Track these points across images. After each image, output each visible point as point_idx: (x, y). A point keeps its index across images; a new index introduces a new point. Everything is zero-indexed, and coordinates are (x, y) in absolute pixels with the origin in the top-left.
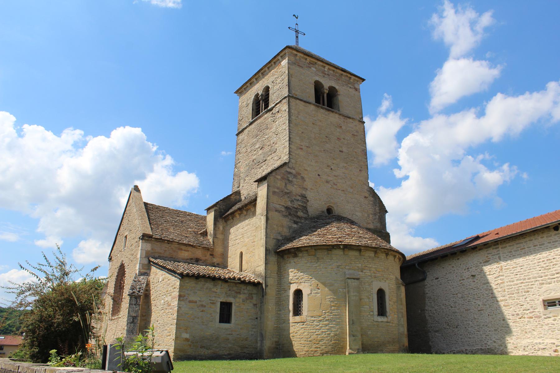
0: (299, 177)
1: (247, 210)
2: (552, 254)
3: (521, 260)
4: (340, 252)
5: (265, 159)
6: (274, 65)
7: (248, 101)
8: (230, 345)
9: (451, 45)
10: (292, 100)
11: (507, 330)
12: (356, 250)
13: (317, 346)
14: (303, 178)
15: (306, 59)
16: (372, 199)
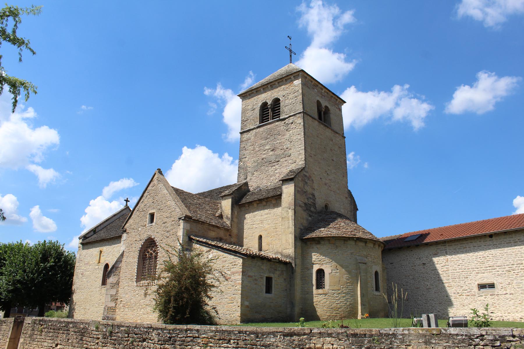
1: (267, 202)
2: (487, 253)
3: (463, 255)
4: (353, 243)
6: (285, 82)
7: (254, 105)
8: (272, 311)
9: (314, 33)
10: (305, 115)
11: (450, 303)
14: (313, 180)
15: (312, 82)
16: (349, 199)
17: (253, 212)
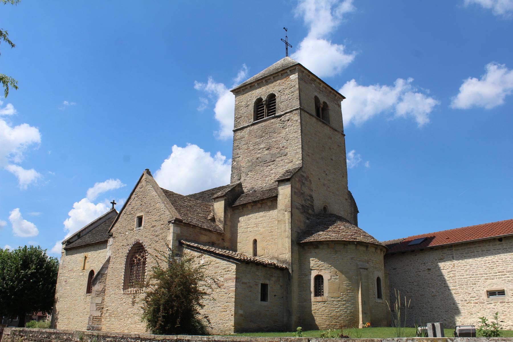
0: (308, 180)
2: (496, 258)
3: (471, 260)
5: (273, 159)
6: (280, 76)
7: (248, 102)
9: (310, 23)
10: (302, 112)
12: (364, 246)
13: (337, 321)
14: (310, 181)
16: (350, 201)
17: (247, 215)
